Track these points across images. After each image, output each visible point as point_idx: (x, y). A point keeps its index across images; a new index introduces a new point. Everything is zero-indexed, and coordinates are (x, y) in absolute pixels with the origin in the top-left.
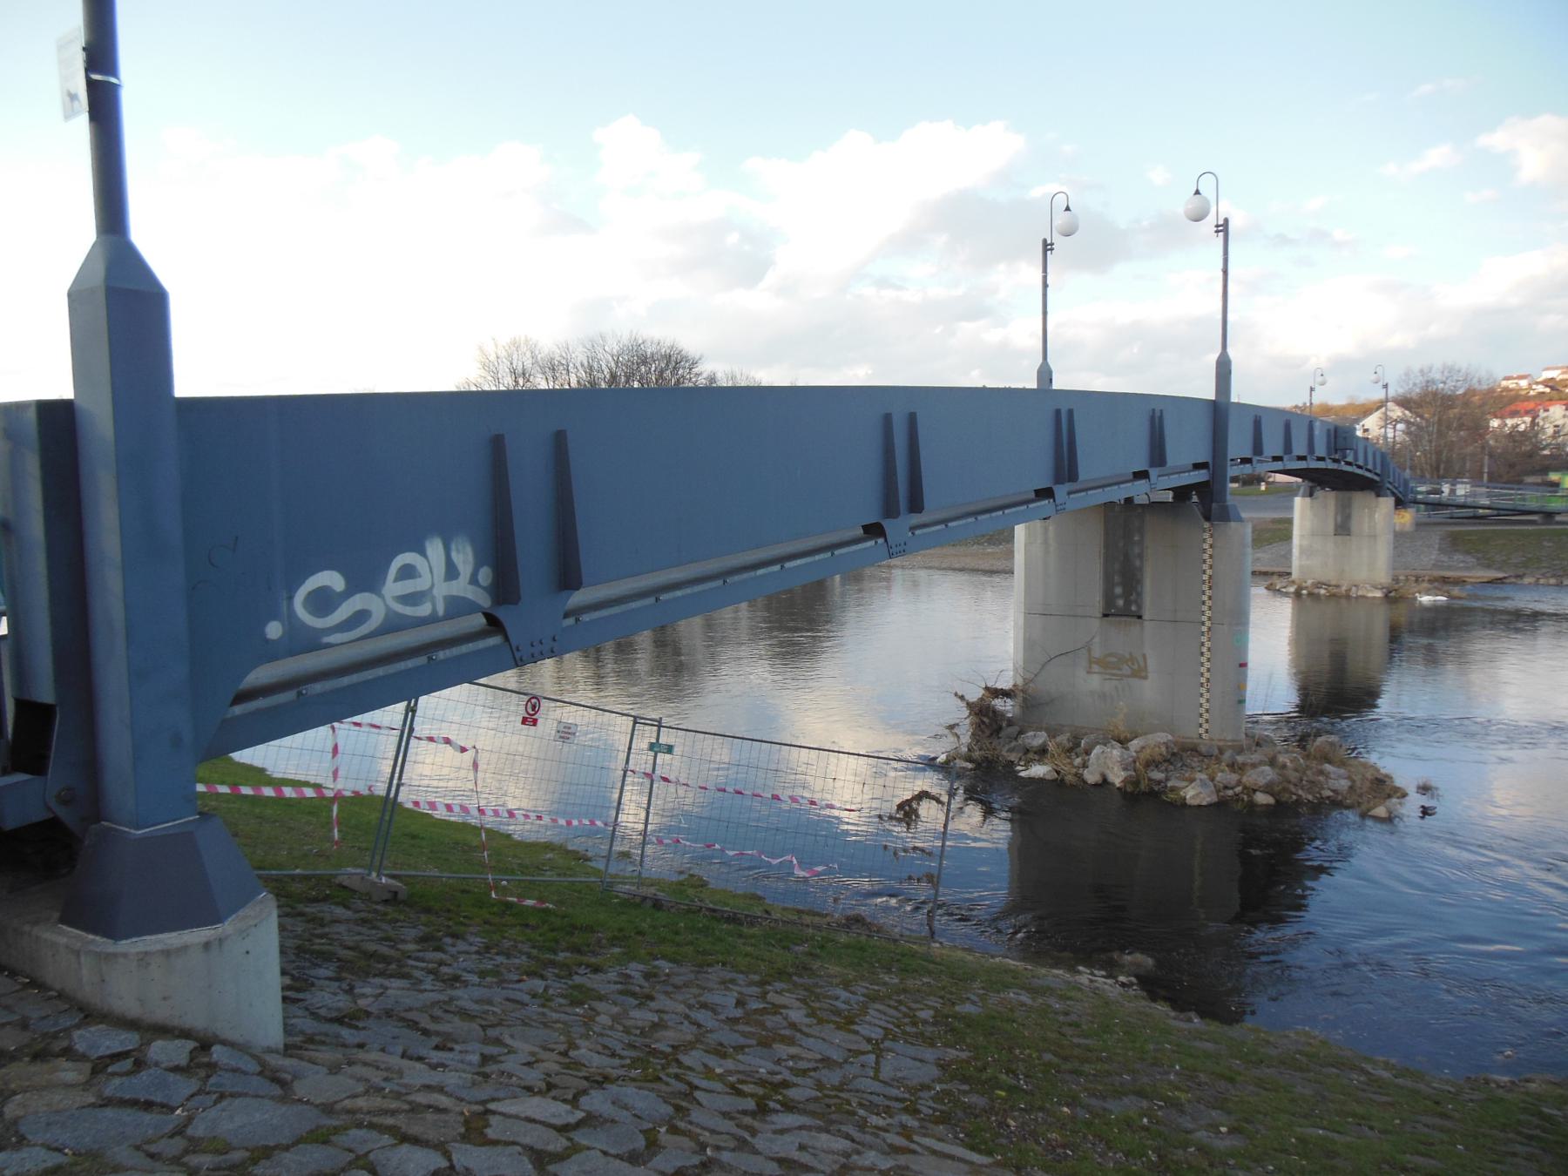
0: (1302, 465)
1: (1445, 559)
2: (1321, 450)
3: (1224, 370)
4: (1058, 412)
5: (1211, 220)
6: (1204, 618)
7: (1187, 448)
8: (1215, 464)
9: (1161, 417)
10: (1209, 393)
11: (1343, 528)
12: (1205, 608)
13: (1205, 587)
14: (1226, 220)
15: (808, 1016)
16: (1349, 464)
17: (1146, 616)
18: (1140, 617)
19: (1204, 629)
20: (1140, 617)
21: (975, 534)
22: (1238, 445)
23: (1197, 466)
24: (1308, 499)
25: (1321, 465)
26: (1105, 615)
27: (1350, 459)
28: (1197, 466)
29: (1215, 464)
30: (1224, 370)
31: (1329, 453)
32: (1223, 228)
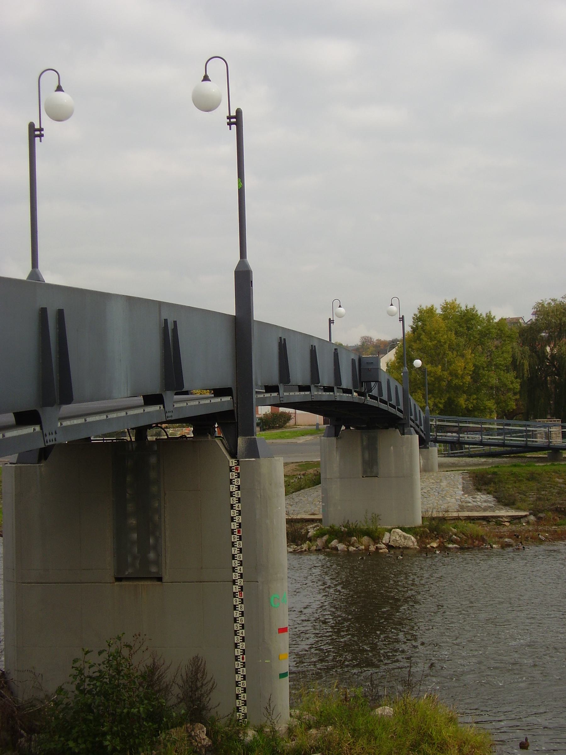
0: (326, 396)
1: (470, 499)
2: (347, 382)
3: (243, 279)
4: (43, 312)
5: (222, 112)
6: (235, 576)
7: (206, 365)
8: (240, 387)
9: (175, 330)
10: (231, 311)
11: (370, 468)
12: (235, 563)
13: (235, 538)
14: (239, 112)
15: (181, 727)
16: (372, 397)
17: (166, 578)
18: (160, 579)
19: (236, 589)
20: (160, 579)
21: (325, 535)
22: (264, 369)
23: (218, 392)
24: (334, 439)
25: (346, 397)
26: (118, 579)
27: (375, 392)
28: (218, 392)
29: (240, 387)
30: (243, 279)
31: (355, 386)
32: (236, 120)
